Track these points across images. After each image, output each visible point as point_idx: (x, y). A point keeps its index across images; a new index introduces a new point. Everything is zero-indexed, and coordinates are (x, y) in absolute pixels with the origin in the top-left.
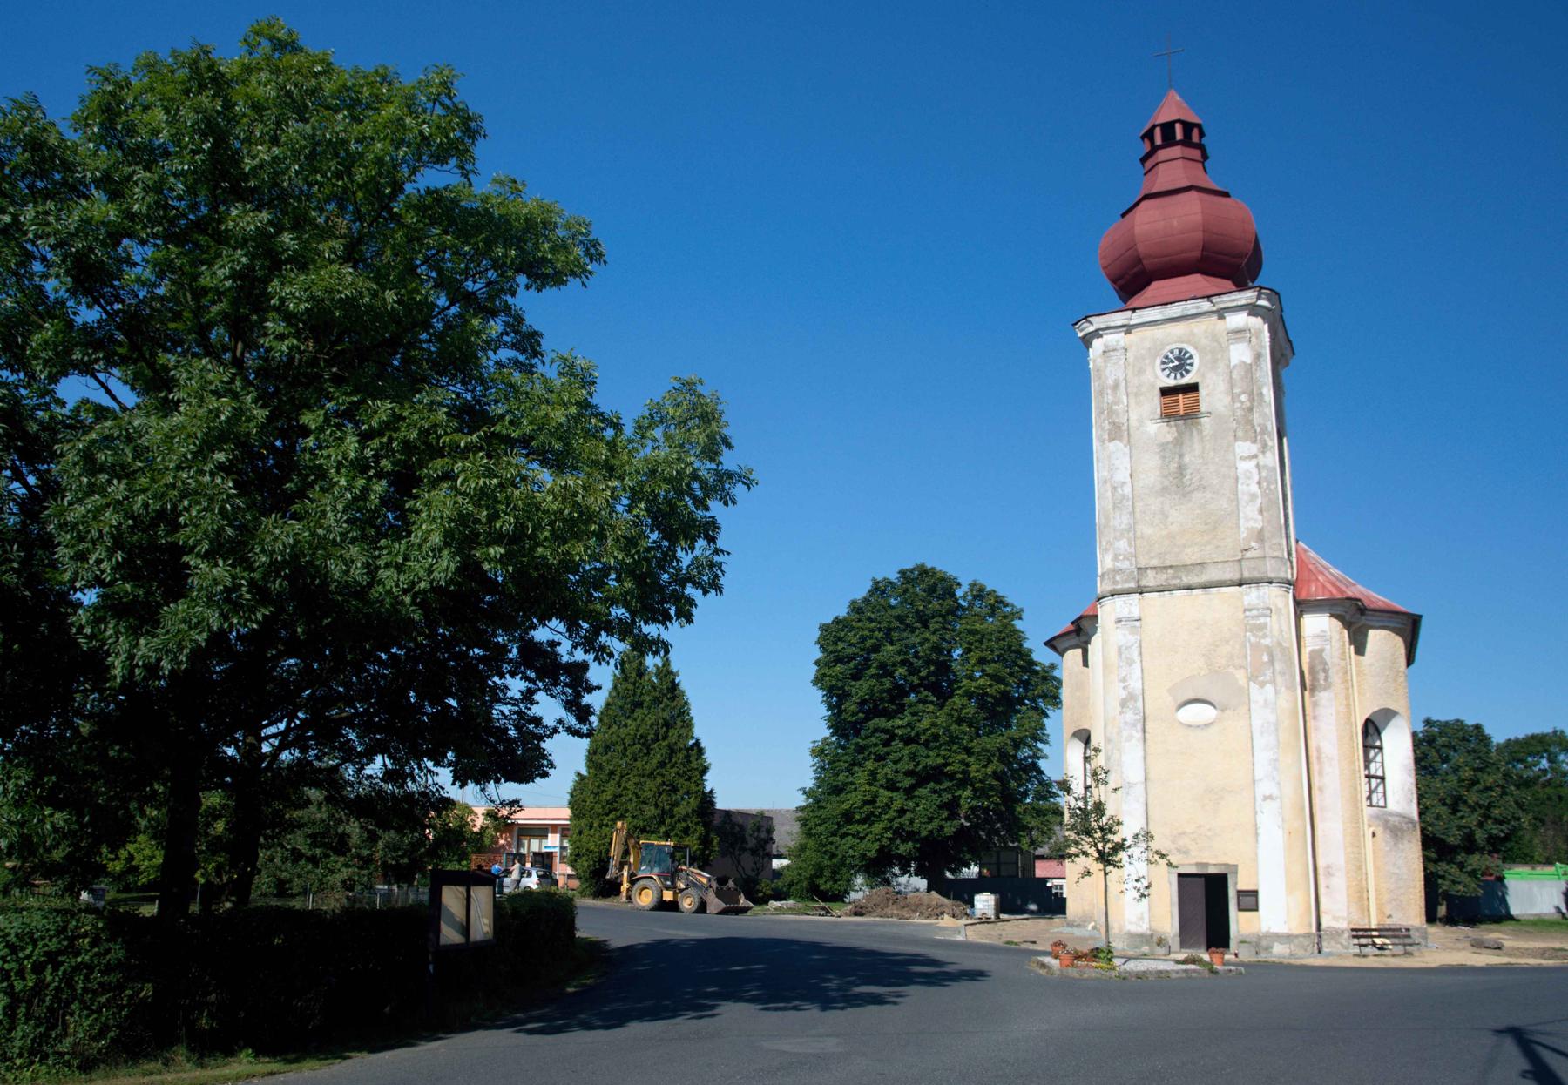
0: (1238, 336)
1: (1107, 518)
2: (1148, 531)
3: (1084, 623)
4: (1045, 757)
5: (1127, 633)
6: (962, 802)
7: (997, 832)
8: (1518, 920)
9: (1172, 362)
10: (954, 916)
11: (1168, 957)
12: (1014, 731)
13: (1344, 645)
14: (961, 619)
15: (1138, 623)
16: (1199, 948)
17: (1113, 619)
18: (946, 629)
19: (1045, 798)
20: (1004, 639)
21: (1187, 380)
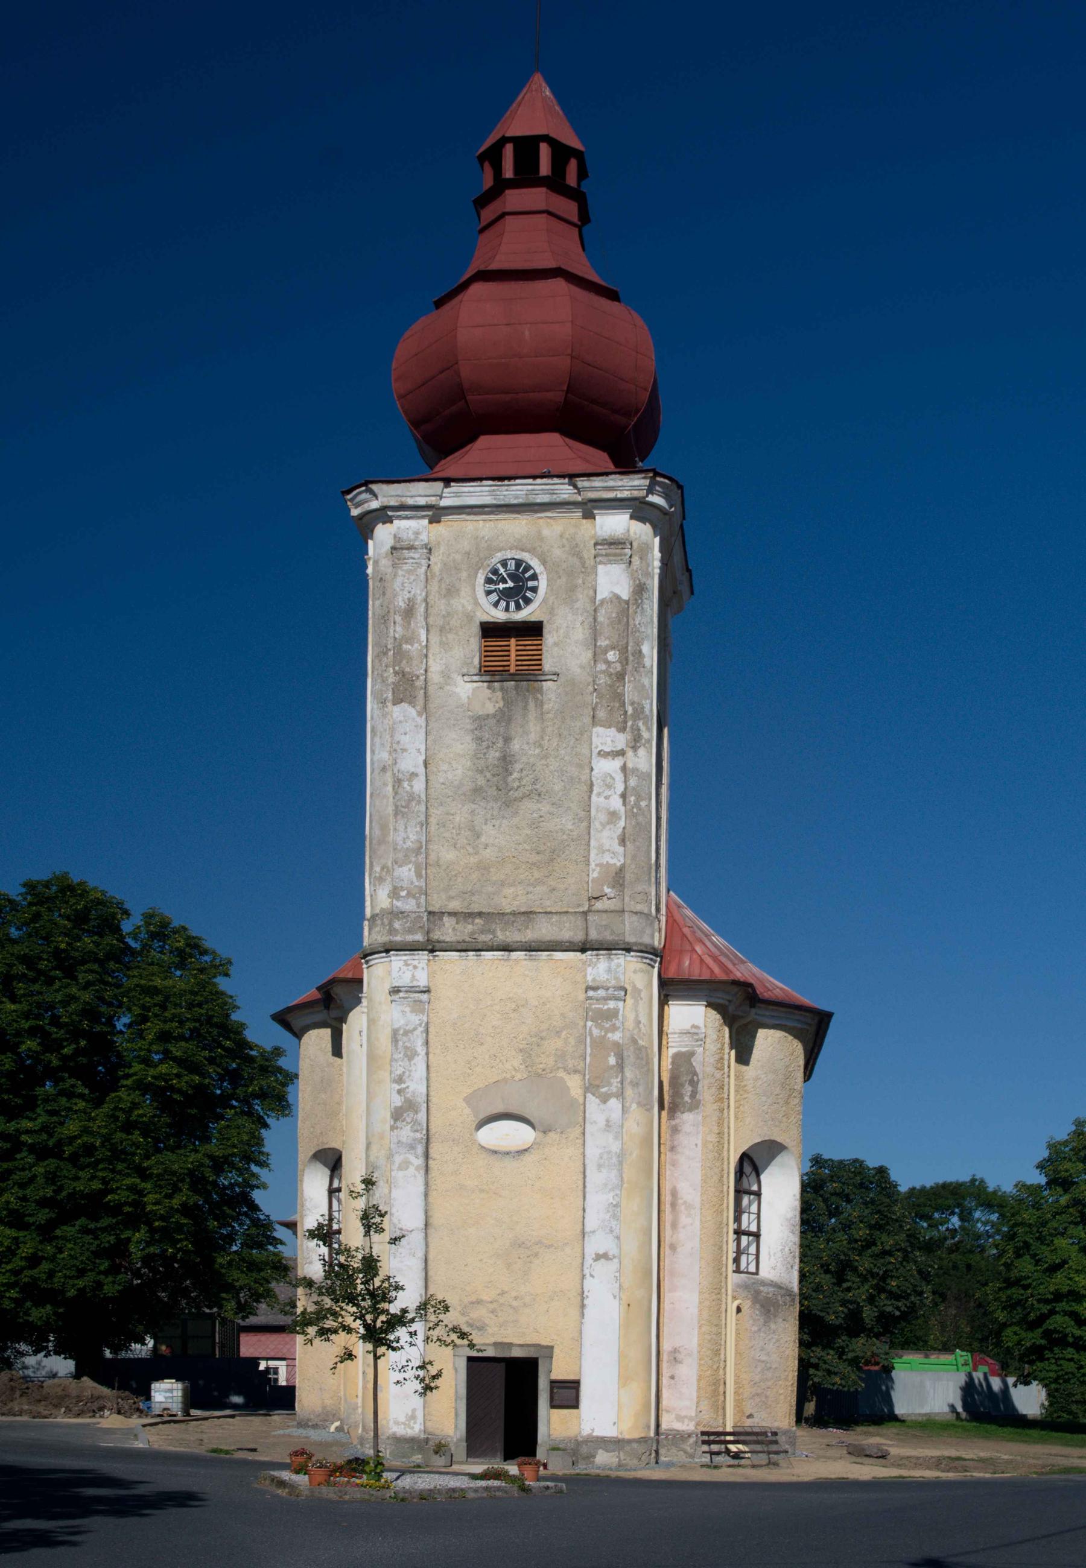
0: (613, 550)
1: (384, 828)
2: (448, 855)
3: (338, 991)
4: (264, 1186)
5: (408, 1009)
6: (132, 1248)
7: (185, 1293)
8: (903, 1421)
9: (504, 581)
10: (119, 1413)
11: (450, 1469)
12: (213, 1147)
13: (722, 1049)
14: (129, 969)
15: (424, 997)
16: (494, 1456)
17: (387, 987)
18: (107, 983)
19: (261, 1246)
20: (200, 1005)
21: (524, 615)
